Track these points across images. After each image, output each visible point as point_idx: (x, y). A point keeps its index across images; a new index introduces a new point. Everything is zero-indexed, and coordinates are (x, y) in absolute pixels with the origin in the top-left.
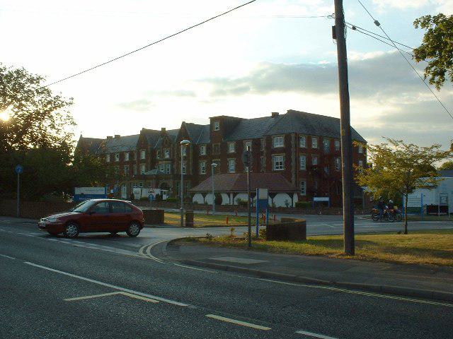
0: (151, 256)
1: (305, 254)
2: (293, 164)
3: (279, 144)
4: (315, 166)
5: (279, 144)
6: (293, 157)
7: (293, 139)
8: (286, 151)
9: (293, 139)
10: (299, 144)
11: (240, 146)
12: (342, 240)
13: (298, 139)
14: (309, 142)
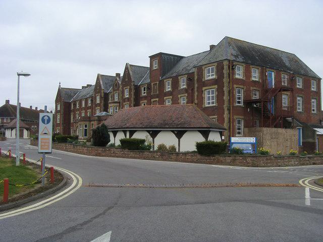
0: (73, 177)
1: (230, 116)
2: (226, 98)
3: (210, 75)
4: (256, 102)
5: (210, 75)
6: (225, 89)
7: (226, 67)
8: (218, 82)
9: (226, 67)
10: (234, 74)
11: (175, 84)
12: (49, 139)
13: (232, 67)
14: (248, 73)
